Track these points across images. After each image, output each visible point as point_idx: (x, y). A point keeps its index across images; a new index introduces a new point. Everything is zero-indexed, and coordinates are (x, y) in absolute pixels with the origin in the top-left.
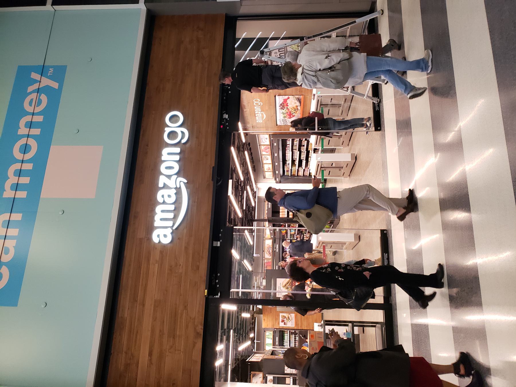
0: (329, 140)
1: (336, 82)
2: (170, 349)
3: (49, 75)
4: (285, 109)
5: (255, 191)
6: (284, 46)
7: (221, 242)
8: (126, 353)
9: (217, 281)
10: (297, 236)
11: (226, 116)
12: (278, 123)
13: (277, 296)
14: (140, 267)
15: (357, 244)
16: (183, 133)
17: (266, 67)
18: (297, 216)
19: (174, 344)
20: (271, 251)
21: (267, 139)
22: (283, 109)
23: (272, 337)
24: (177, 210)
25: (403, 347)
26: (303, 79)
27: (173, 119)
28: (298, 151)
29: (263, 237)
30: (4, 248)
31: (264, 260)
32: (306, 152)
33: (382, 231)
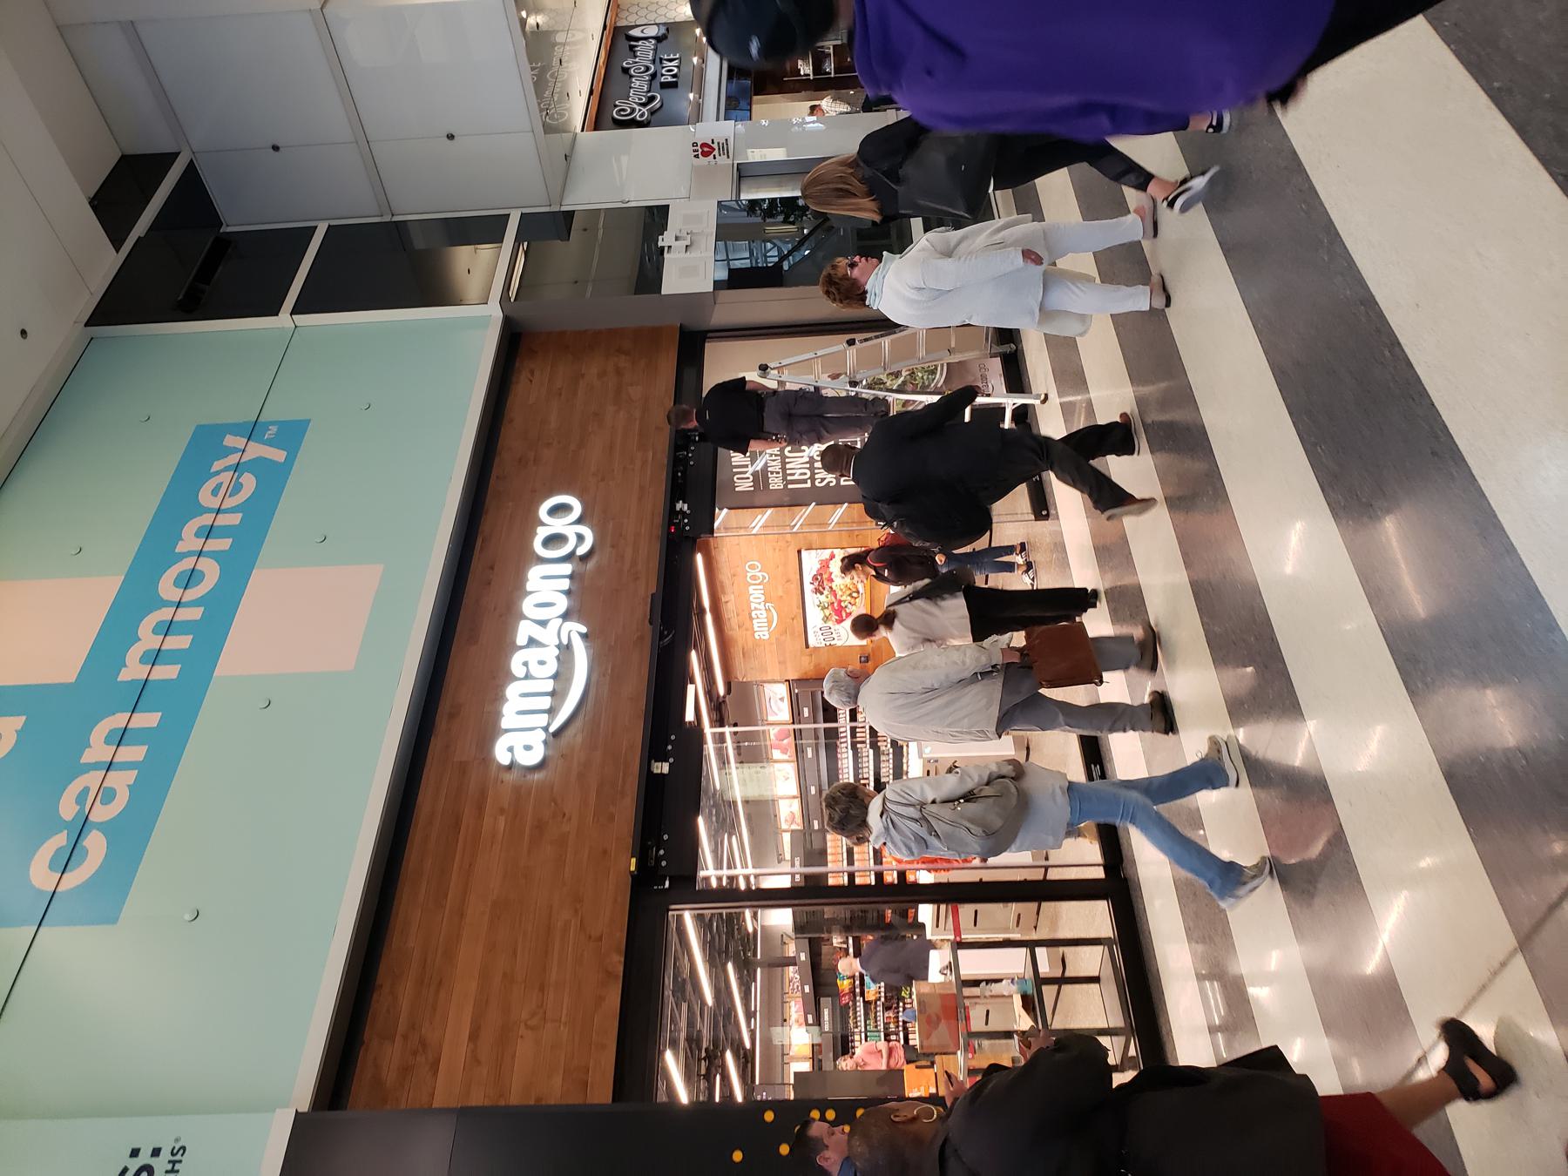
0: (976, 912)
1: (984, 831)
4: (826, 592)
8: (405, 1037)
9: (662, 852)
10: (886, 1015)
12: (812, 642)
14: (457, 825)
19: (542, 1005)
21: (782, 699)
22: (822, 593)
24: (557, 695)
26: (887, 829)
28: (871, 748)
29: (783, 1055)
32: (891, 750)
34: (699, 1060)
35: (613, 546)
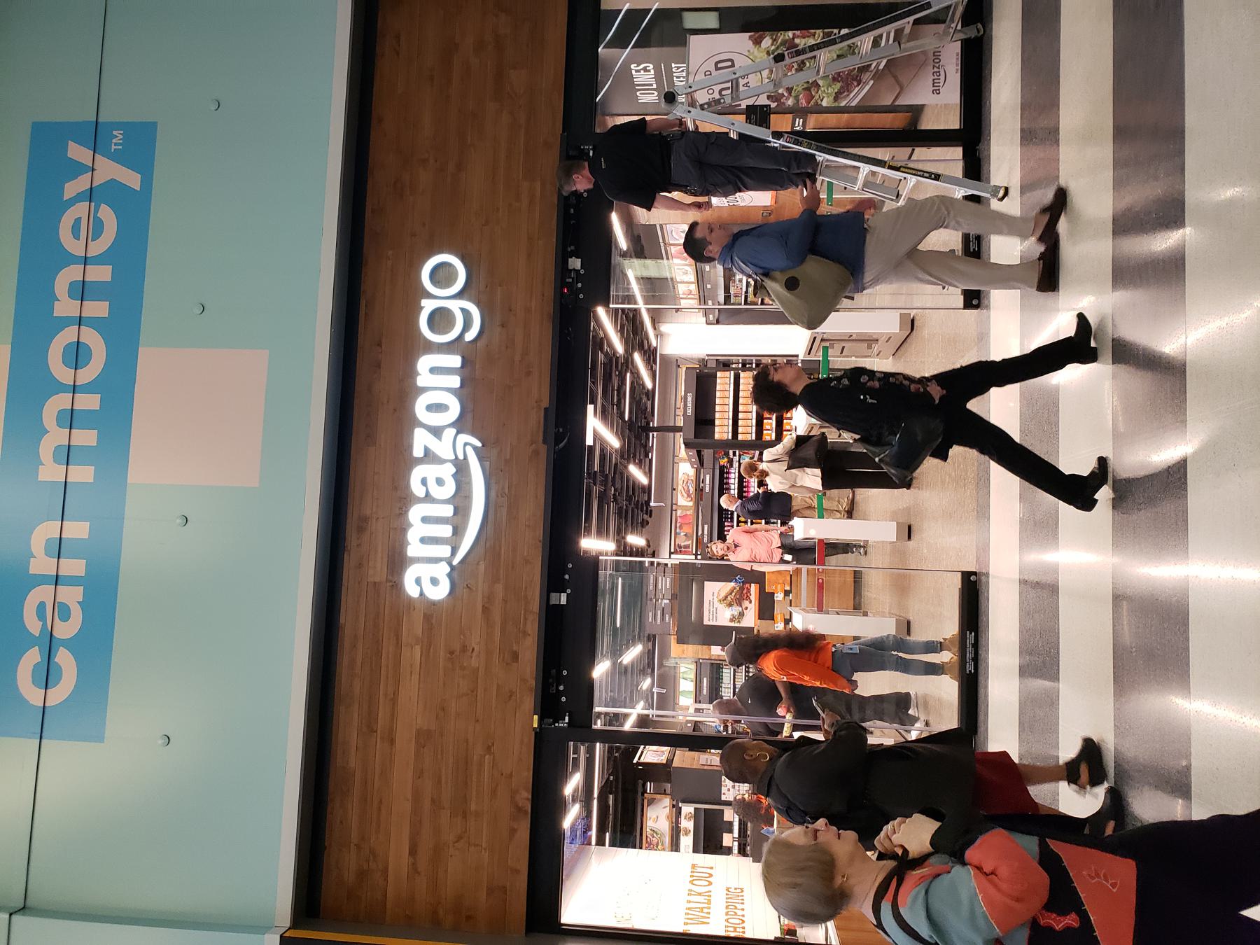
2: (457, 842)
3: (113, 151)
5: (655, 346)
6: (731, 78)
7: (568, 594)
9: (561, 688)
11: (575, 263)
13: (705, 623)
15: (908, 336)
16: (466, 313)
17: (681, 139)
18: (766, 288)
20: (692, 490)
23: (692, 676)
24: (458, 531)
25: (1000, 429)
27: (440, 273)
30: (56, 605)
31: (676, 510)
33: (966, 576)
34: (613, 405)
35: (503, 326)
